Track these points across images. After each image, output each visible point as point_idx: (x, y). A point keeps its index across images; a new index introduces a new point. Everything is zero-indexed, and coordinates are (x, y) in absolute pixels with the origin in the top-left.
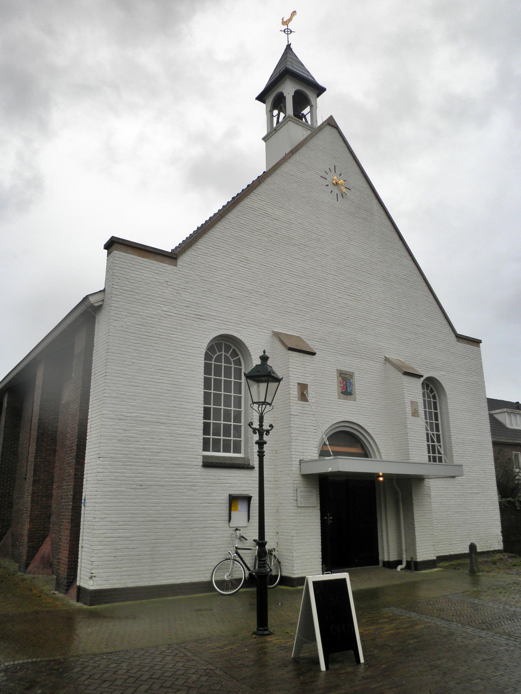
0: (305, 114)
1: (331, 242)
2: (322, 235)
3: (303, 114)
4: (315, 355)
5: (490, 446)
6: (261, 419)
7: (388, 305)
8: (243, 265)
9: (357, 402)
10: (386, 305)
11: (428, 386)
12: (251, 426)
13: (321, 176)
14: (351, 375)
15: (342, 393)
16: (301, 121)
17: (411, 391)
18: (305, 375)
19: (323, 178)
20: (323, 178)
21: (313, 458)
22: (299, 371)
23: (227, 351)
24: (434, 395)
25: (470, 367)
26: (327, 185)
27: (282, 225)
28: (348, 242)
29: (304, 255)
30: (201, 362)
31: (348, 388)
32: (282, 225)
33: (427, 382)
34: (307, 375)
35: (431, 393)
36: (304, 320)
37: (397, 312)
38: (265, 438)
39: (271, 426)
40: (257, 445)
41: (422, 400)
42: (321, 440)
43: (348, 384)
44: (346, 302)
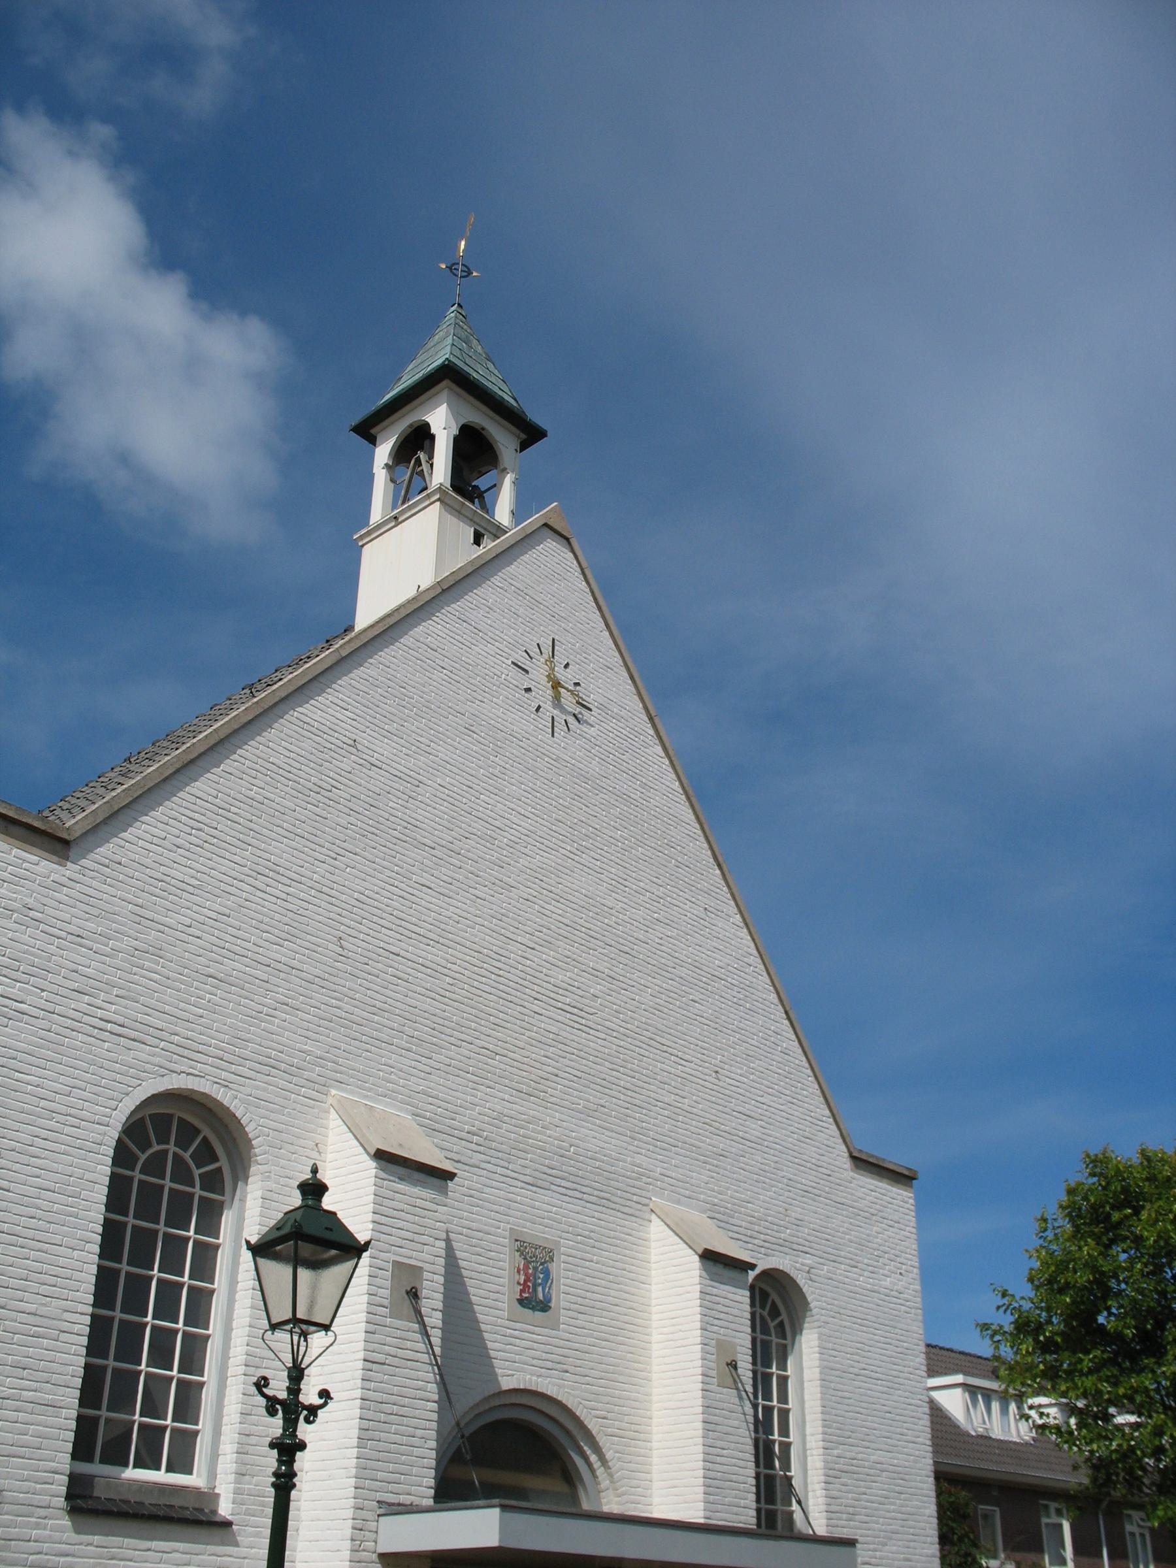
0: (483, 490)
1: (523, 850)
2: (502, 826)
3: (476, 487)
4: (452, 1180)
5: (928, 1486)
6: (297, 1374)
7: (670, 1050)
8: (263, 887)
9: (560, 1333)
10: (665, 1048)
11: (764, 1295)
12: (264, 1390)
13: (513, 663)
14: (549, 1255)
15: (522, 1302)
16: (478, 528)
17: (720, 1307)
18: (416, 1238)
19: (520, 667)
20: (520, 667)
21: (416, 1501)
22: (401, 1224)
23: (183, 1144)
24: (781, 1324)
25: (882, 1248)
26: (528, 690)
27: (390, 783)
28: (572, 856)
29: (445, 878)
30: (103, 1170)
31: (540, 1289)
32: (390, 783)
33: (764, 1286)
34: (425, 1239)
35: (773, 1319)
36: (428, 1069)
37: (693, 1072)
38: (304, 1431)
39: (325, 1394)
40: (276, 1451)
41: (750, 1338)
42: (446, 1446)
43: (541, 1276)
44: (554, 1029)
